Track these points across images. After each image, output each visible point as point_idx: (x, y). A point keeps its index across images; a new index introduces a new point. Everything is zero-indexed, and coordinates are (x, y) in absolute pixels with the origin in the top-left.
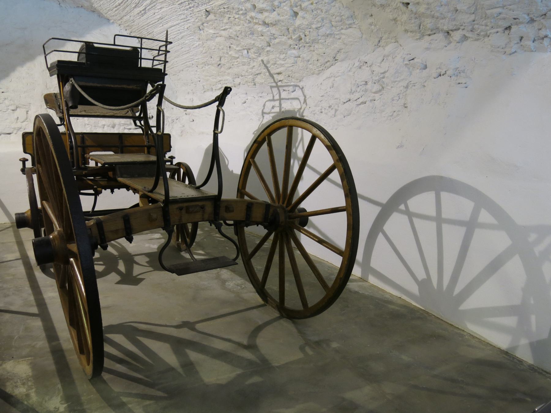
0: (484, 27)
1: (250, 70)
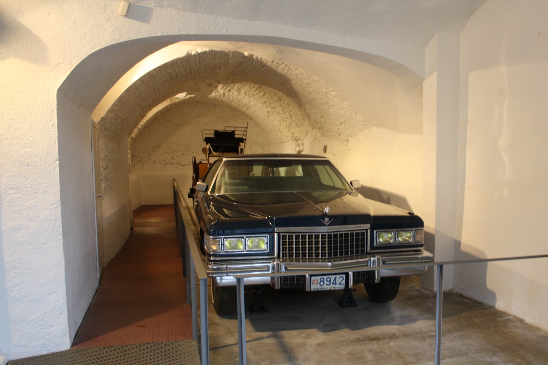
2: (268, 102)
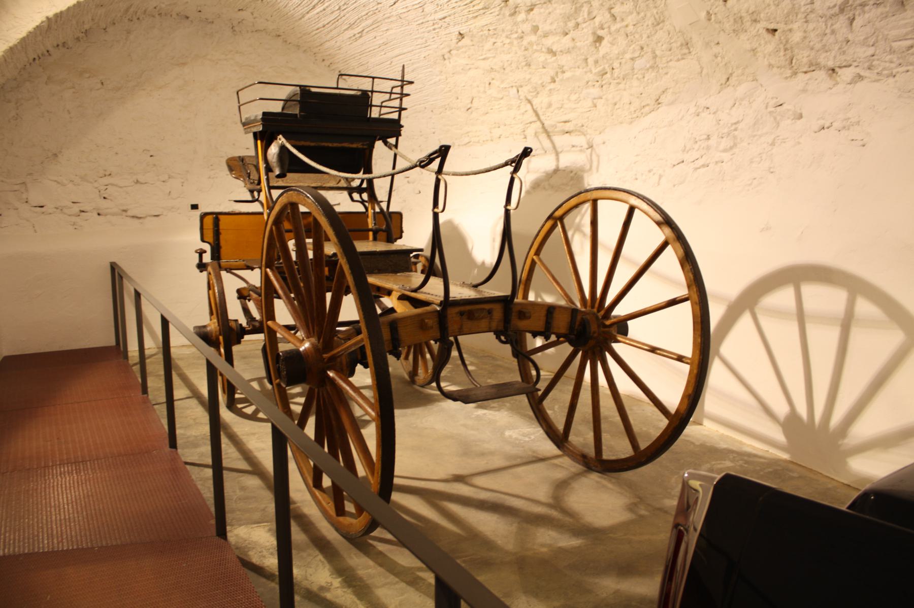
0: (888, 64)
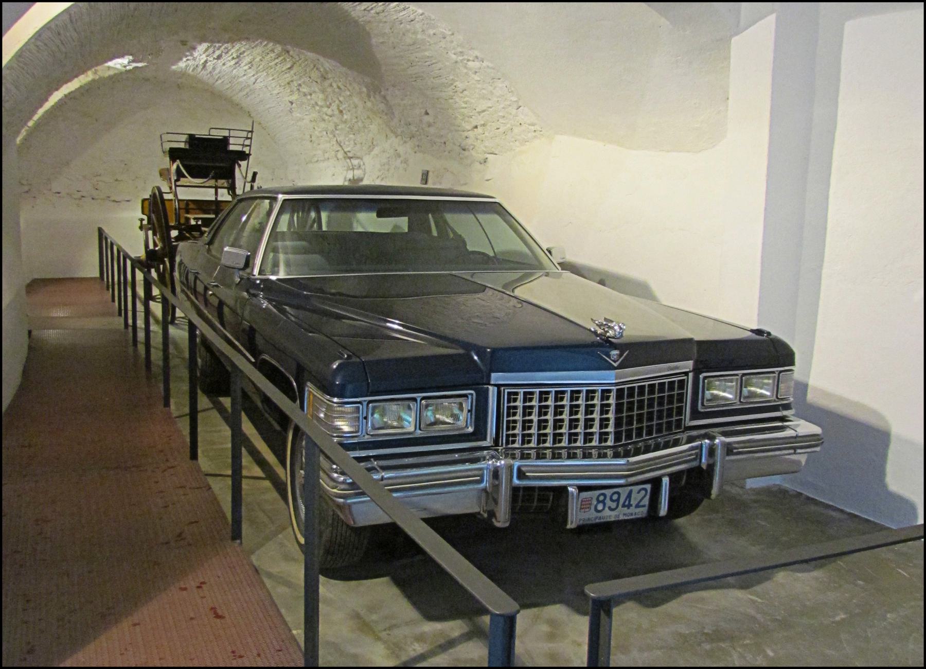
1: (332, 148)
2: (295, 84)
